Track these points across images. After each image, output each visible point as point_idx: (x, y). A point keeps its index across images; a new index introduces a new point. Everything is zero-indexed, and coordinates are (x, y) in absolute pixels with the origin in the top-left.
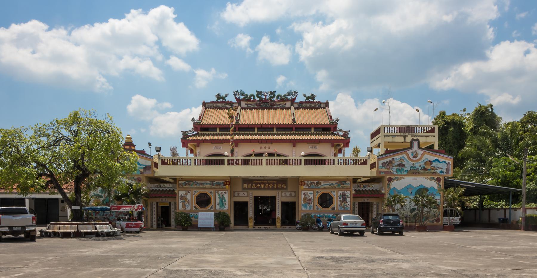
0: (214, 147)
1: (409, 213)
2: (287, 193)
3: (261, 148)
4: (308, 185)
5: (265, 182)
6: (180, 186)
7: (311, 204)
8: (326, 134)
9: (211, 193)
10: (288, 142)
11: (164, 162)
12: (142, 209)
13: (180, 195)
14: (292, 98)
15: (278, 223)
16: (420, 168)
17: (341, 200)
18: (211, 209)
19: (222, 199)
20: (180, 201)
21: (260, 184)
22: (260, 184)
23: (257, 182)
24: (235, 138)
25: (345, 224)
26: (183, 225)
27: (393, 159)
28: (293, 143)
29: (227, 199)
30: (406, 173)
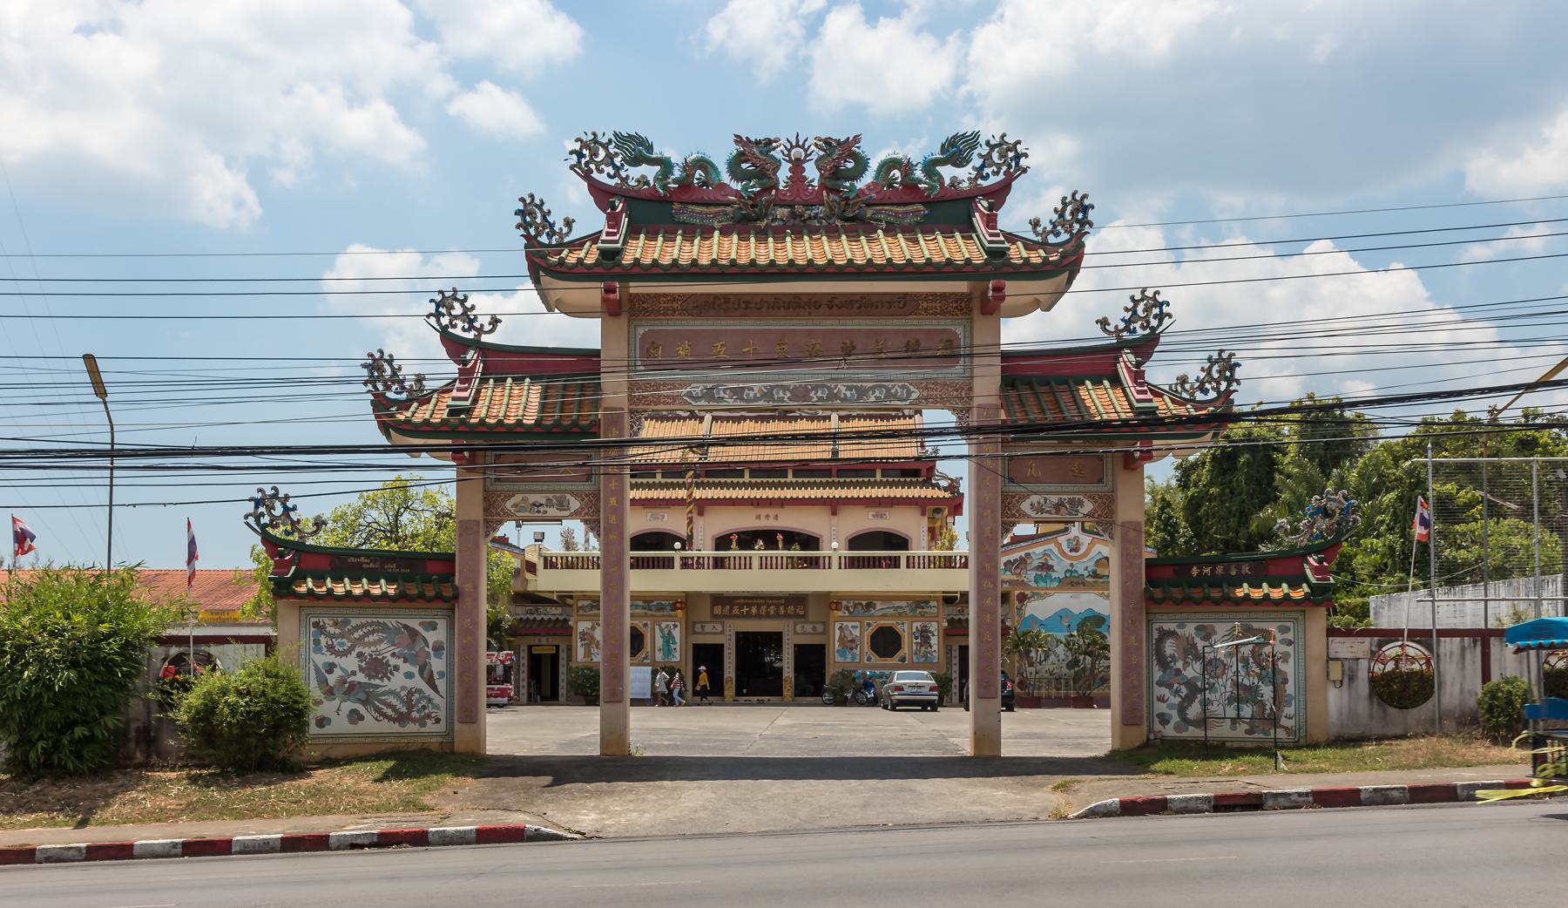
0: (649, 515)
1: (1065, 670)
2: (806, 626)
3: (759, 517)
4: (847, 608)
5: (759, 601)
6: (581, 612)
7: (855, 651)
8: (910, 485)
9: (645, 625)
10: (824, 504)
11: (549, 563)
12: (511, 660)
13: (580, 630)
14: (980, 182)
15: (788, 689)
16: (1086, 574)
17: (919, 641)
18: (646, 661)
19: (668, 638)
20: (579, 644)
21: (749, 606)
22: (749, 606)
23: (742, 601)
24: (698, 494)
25: (899, 688)
26: (587, 694)
27: (1028, 555)
28: (831, 505)
29: (678, 640)
30: (1055, 584)
